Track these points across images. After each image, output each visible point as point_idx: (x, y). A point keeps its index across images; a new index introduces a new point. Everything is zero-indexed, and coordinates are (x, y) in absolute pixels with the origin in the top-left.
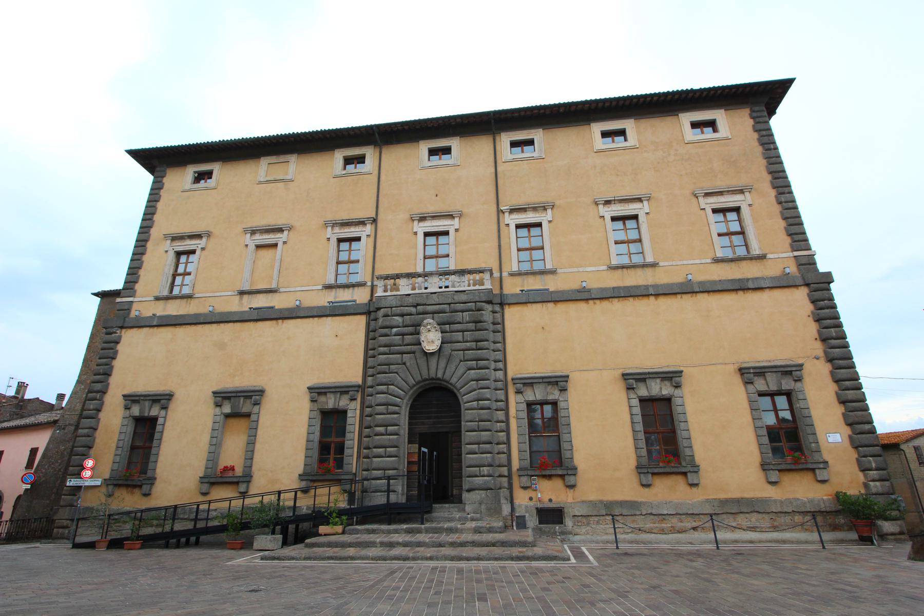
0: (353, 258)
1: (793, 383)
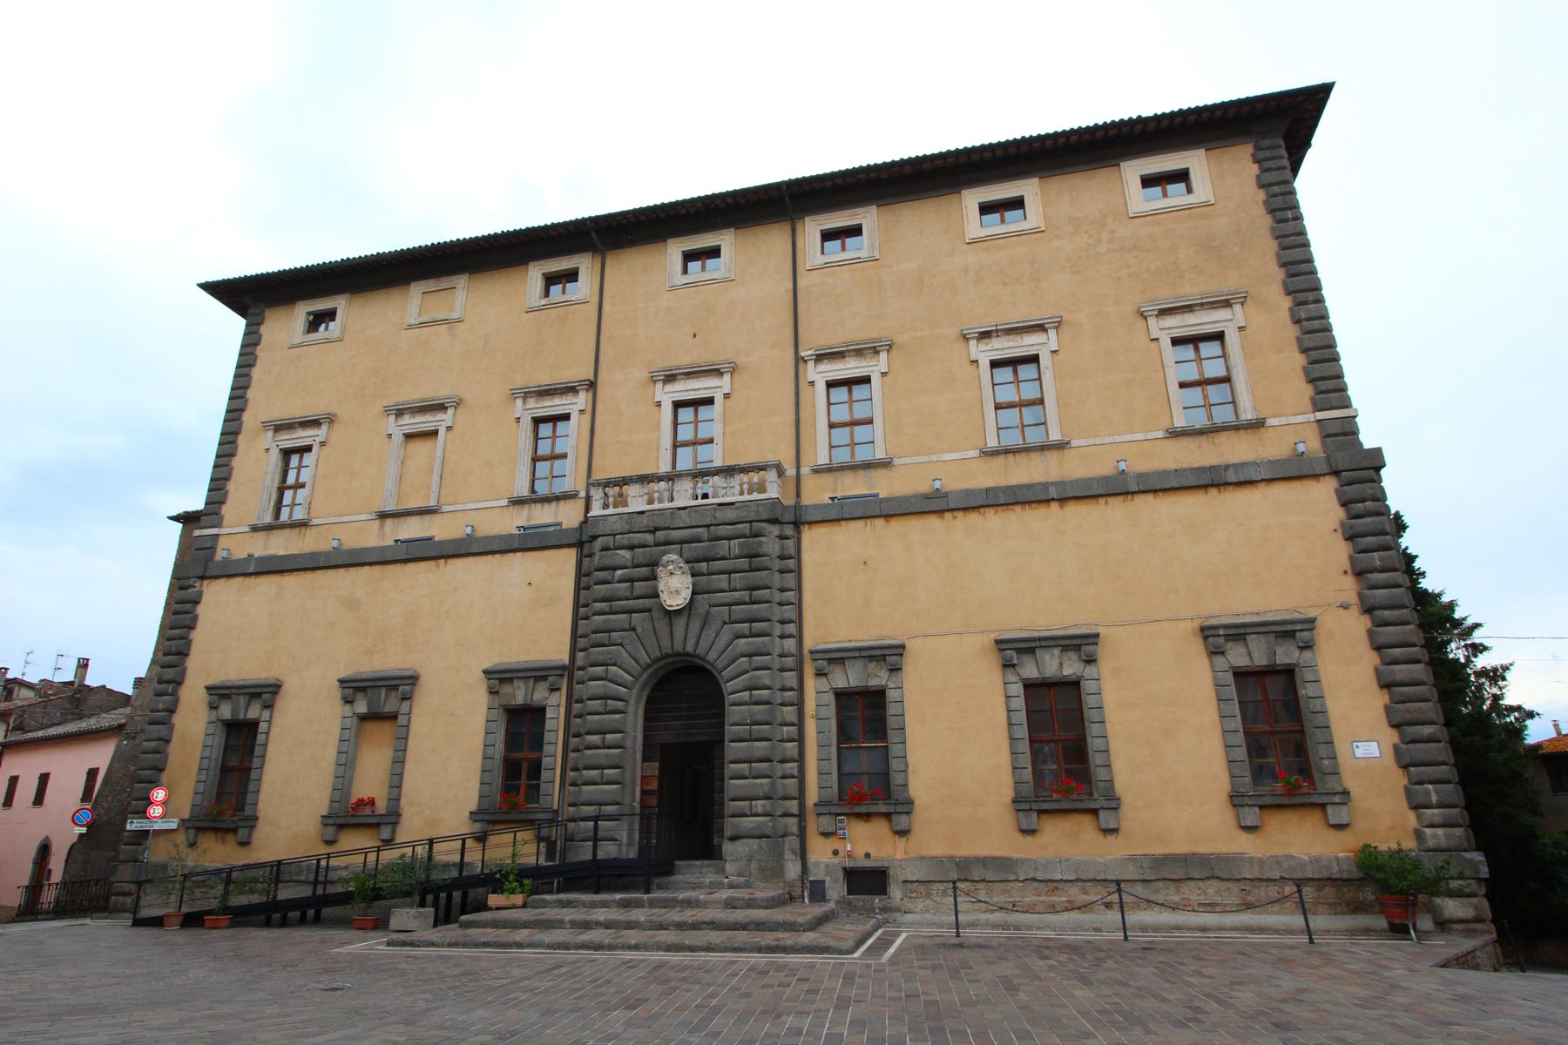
1: (1296, 652)
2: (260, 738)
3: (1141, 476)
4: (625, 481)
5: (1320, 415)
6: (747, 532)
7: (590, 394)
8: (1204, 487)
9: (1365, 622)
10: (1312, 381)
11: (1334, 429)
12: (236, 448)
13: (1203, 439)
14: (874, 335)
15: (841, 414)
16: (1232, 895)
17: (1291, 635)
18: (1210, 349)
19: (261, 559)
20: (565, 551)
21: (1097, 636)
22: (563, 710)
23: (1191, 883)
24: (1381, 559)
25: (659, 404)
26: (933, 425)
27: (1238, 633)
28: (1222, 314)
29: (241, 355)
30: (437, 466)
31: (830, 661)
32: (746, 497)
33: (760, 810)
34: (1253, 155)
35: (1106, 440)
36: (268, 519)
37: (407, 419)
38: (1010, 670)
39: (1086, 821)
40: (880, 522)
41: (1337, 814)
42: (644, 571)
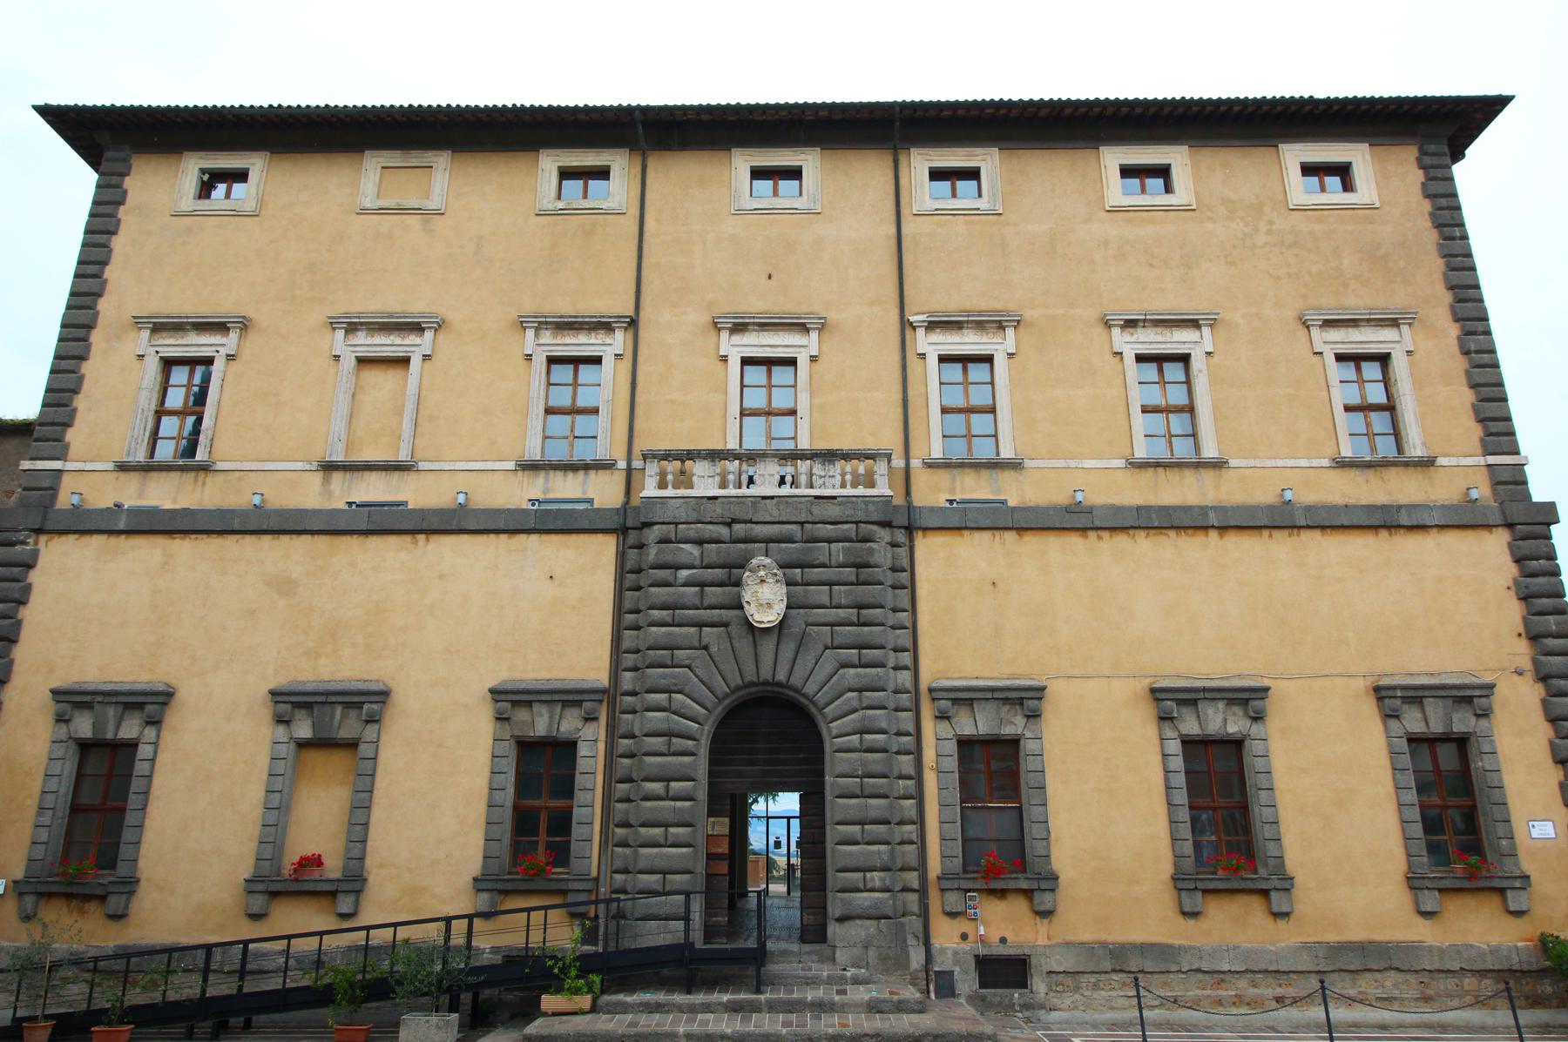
1: (1473, 720)
2: (140, 768)
3: (1309, 509)
4: (691, 455)
5: (1492, 460)
6: (853, 535)
7: (630, 335)
8: (1375, 528)
10: (1481, 420)
11: (1506, 477)
12: (88, 348)
13: (1371, 472)
14: (998, 306)
15: (756, 399)
16: (1408, 987)
17: (1469, 700)
18: (1173, 372)
19: (135, 512)
20: (600, 538)
21: (1267, 689)
22: (601, 746)
23: (1367, 975)
24: (1557, 624)
25: (724, 359)
26: (1071, 423)
27: (1415, 696)
28: (1389, 334)
29: (92, 215)
30: (410, 407)
31: (515, 703)
32: (849, 491)
33: (877, 884)
34: (1419, 160)
35: (1269, 463)
36: (141, 456)
37: (361, 338)
38: (1167, 724)
39: (1255, 903)
40: (1010, 536)
41: (1515, 900)
42: (719, 573)
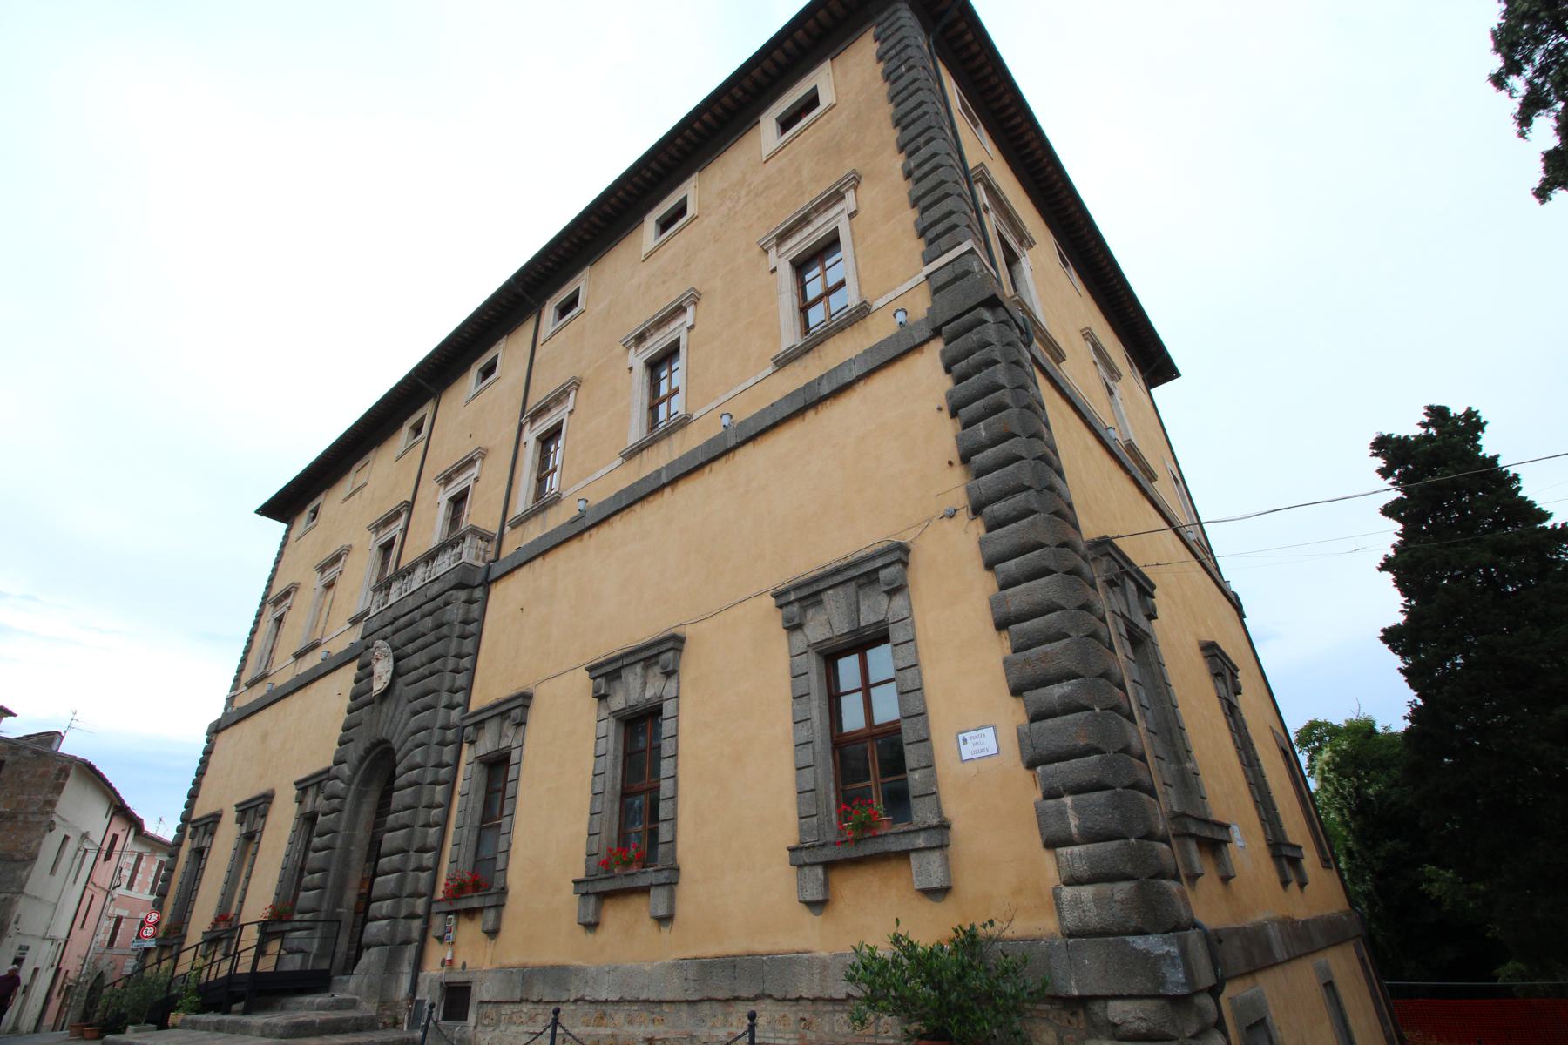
0: (831, 283)
1: (884, 600)
8: (801, 412)
9: (977, 528)
17: (870, 578)
